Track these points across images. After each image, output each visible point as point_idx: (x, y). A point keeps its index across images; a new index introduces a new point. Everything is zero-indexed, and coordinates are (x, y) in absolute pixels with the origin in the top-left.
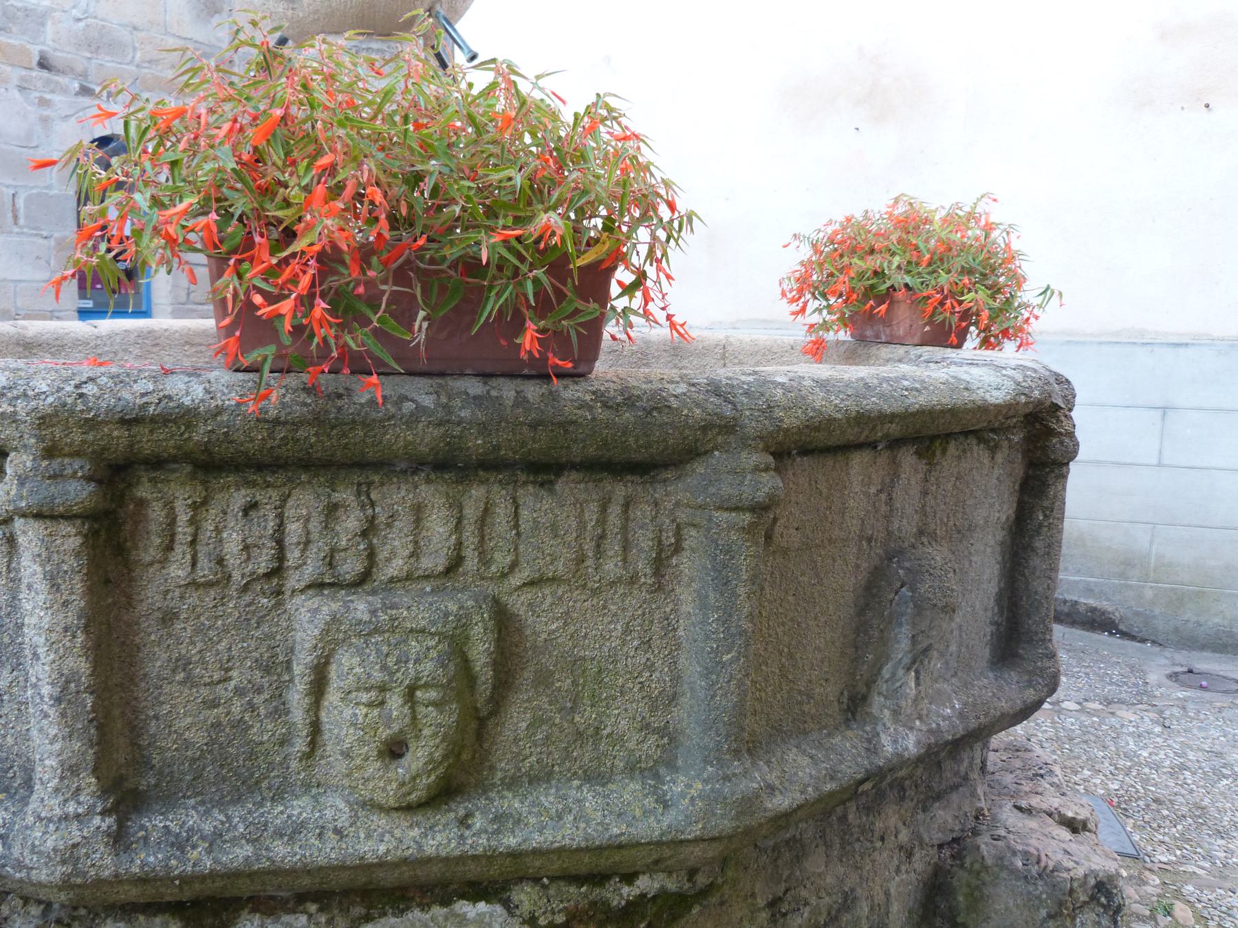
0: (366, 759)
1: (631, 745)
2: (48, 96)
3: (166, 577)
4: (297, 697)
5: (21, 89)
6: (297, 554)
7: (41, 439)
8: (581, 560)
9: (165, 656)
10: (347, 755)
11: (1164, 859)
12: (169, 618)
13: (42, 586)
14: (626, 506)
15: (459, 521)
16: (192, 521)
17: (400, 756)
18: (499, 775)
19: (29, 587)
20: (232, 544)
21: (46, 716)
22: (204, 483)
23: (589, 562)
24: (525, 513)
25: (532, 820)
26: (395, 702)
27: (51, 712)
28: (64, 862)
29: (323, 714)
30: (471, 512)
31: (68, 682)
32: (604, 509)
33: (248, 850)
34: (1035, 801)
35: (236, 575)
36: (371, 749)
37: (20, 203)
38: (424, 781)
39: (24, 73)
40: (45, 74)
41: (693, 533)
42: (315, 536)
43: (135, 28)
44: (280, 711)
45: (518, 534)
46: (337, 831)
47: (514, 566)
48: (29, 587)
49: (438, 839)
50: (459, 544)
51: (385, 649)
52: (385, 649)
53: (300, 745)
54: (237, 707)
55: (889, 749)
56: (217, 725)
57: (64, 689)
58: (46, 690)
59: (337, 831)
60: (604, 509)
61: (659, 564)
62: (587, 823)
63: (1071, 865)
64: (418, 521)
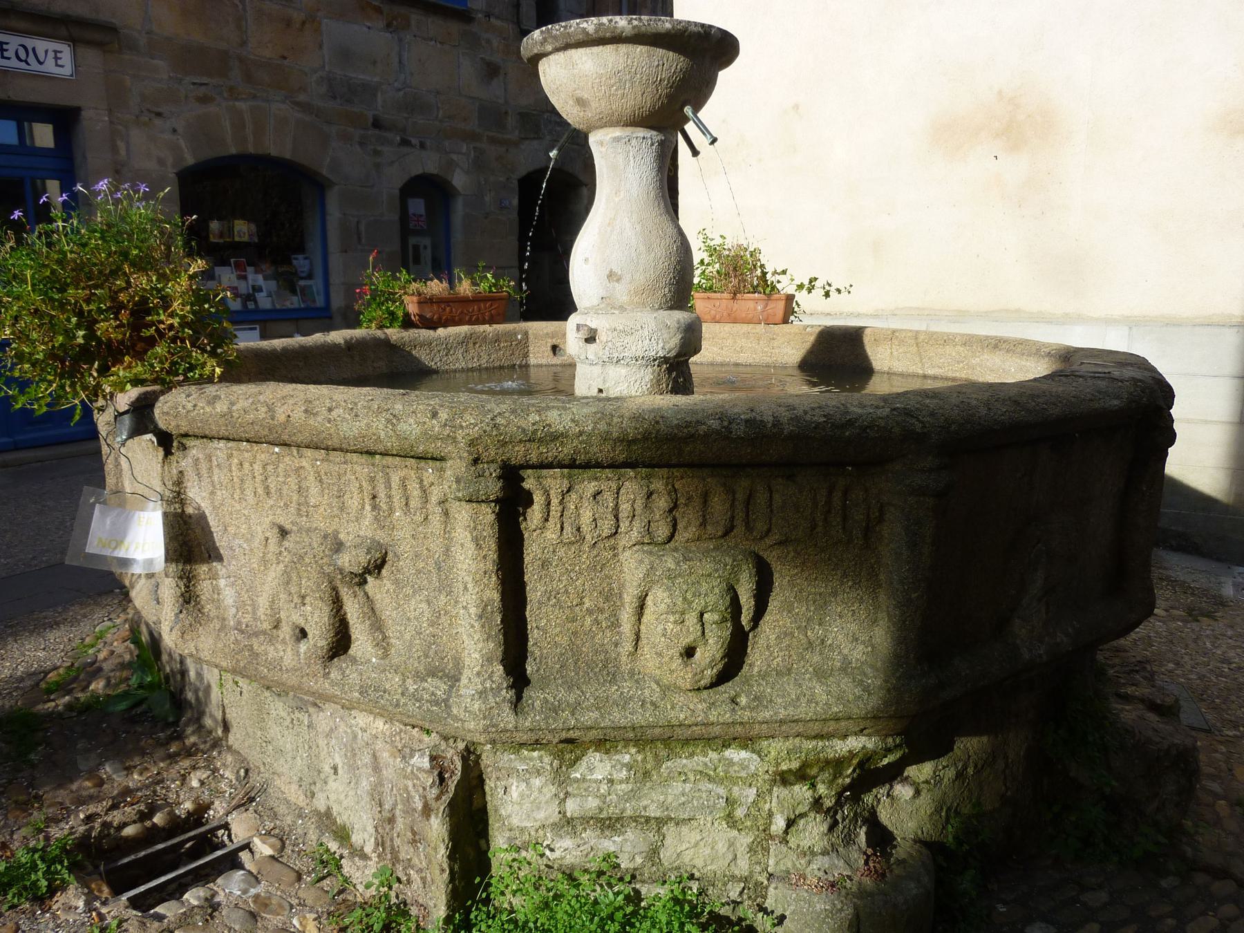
0: (672, 658)
1: (846, 651)
2: (379, 148)
3: (540, 537)
4: (626, 617)
5: (361, 144)
6: (627, 524)
7: (470, 453)
8: (813, 527)
9: (543, 589)
10: (660, 654)
11: (1231, 733)
12: (545, 564)
13: (471, 546)
14: (846, 493)
15: (734, 500)
16: (561, 502)
17: (693, 656)
18: (756, 669)
19: (462, 545)
20: (586, 516)
21: (473, 626)
22: (570, 477)
23: (819, 529)
24: (776, 496)
25: (780, 701)
26: (692, 619)
27: (476, 625)
28: (485, 718)
29: (642, 627)
30: (740, 496)
31: (486, 606)
32: (830, 493)
33: (595, 715)
34: (1130, 690)
35: (588, 537)
36: (675, 652)
37: (362, 228)
38: (709, 672)
39: (362, 132)
40: (377, 132)
41: (892, 509)
42: (639, 511)
43: (438, 93)
44: (615, 624)
45: (772, 511)
46: (653, 703)
47: (769, 530)
48: (462, 545)
49: (721, 714)
50: (733, 517)
51: (685, 587)
52: (685, 587)
53: (628, 646)
54: (588, 621)
55: (1027, 656)
56: (575, 633)
57: (484, 609)
58: (473, 610)
59: (653, 703)
60: (830, 493)
61: (867, 532)
62: (817, 703)
63: (1158, 739)
64: (705, 502)
